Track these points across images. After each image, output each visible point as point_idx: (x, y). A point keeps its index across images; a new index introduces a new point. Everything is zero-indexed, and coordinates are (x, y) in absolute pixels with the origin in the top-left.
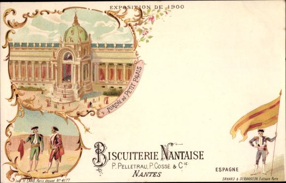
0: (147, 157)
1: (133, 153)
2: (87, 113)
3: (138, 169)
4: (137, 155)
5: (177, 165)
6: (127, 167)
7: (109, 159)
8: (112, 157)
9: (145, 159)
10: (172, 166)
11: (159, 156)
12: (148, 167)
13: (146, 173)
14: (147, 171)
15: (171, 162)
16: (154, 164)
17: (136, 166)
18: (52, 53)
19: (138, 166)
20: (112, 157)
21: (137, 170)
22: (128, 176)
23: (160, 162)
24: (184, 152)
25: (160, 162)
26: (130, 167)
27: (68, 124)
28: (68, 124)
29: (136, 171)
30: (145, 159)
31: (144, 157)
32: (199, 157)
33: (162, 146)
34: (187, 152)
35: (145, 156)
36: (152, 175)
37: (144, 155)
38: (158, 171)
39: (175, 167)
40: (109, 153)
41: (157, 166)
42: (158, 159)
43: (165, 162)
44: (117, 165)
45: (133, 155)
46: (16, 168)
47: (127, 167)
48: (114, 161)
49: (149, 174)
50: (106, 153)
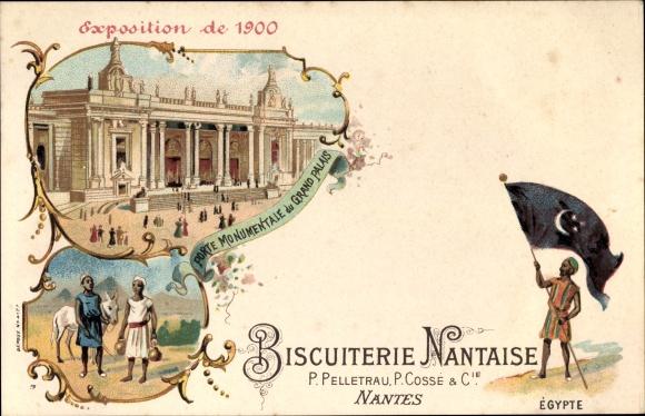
0: (382, 360)
1: (350, 349)
2: (147, 244)
3: (369, 387)
4: (360, 356)
5: (458, 380)
6: (343, 381)
7: (289, 364)
8: (294, 358)
9: (379, 363)
10: (446, 381)
11: (419, 354)
12: (392, 381)
13: (386, 396)
14: (389, 390)
15: (452, 371)
16: (404, 376)
17: (364, 380)
18: (140, 104)
19: (369, 380)
20: (294, 358)
21: (366, 388)
22: (345, 400)
23: (418, 370)
24: (486, 349)
25: (418, 370)
26: (349, 381)
27: (604, 307)
28: (604, 307)
29: (363, 392)
30: (379, 363)
31: (375, 359)
32: (524, 361)
33: (428, 329)
34: (494, 350)
35: (379, 356)
36: (402, 399)
37: (375, 353)
38: (414, 390)
39: (453, 382)
40: (289, 350)
41: (411, 379)
42: (413, 364)
43: (435, 369)
44: (320, 377)
45: (349, 355)
46: (176, 369)
47: (343, 381)
48: (314, 369)
49: (394, 400)
50: (281, 349)
